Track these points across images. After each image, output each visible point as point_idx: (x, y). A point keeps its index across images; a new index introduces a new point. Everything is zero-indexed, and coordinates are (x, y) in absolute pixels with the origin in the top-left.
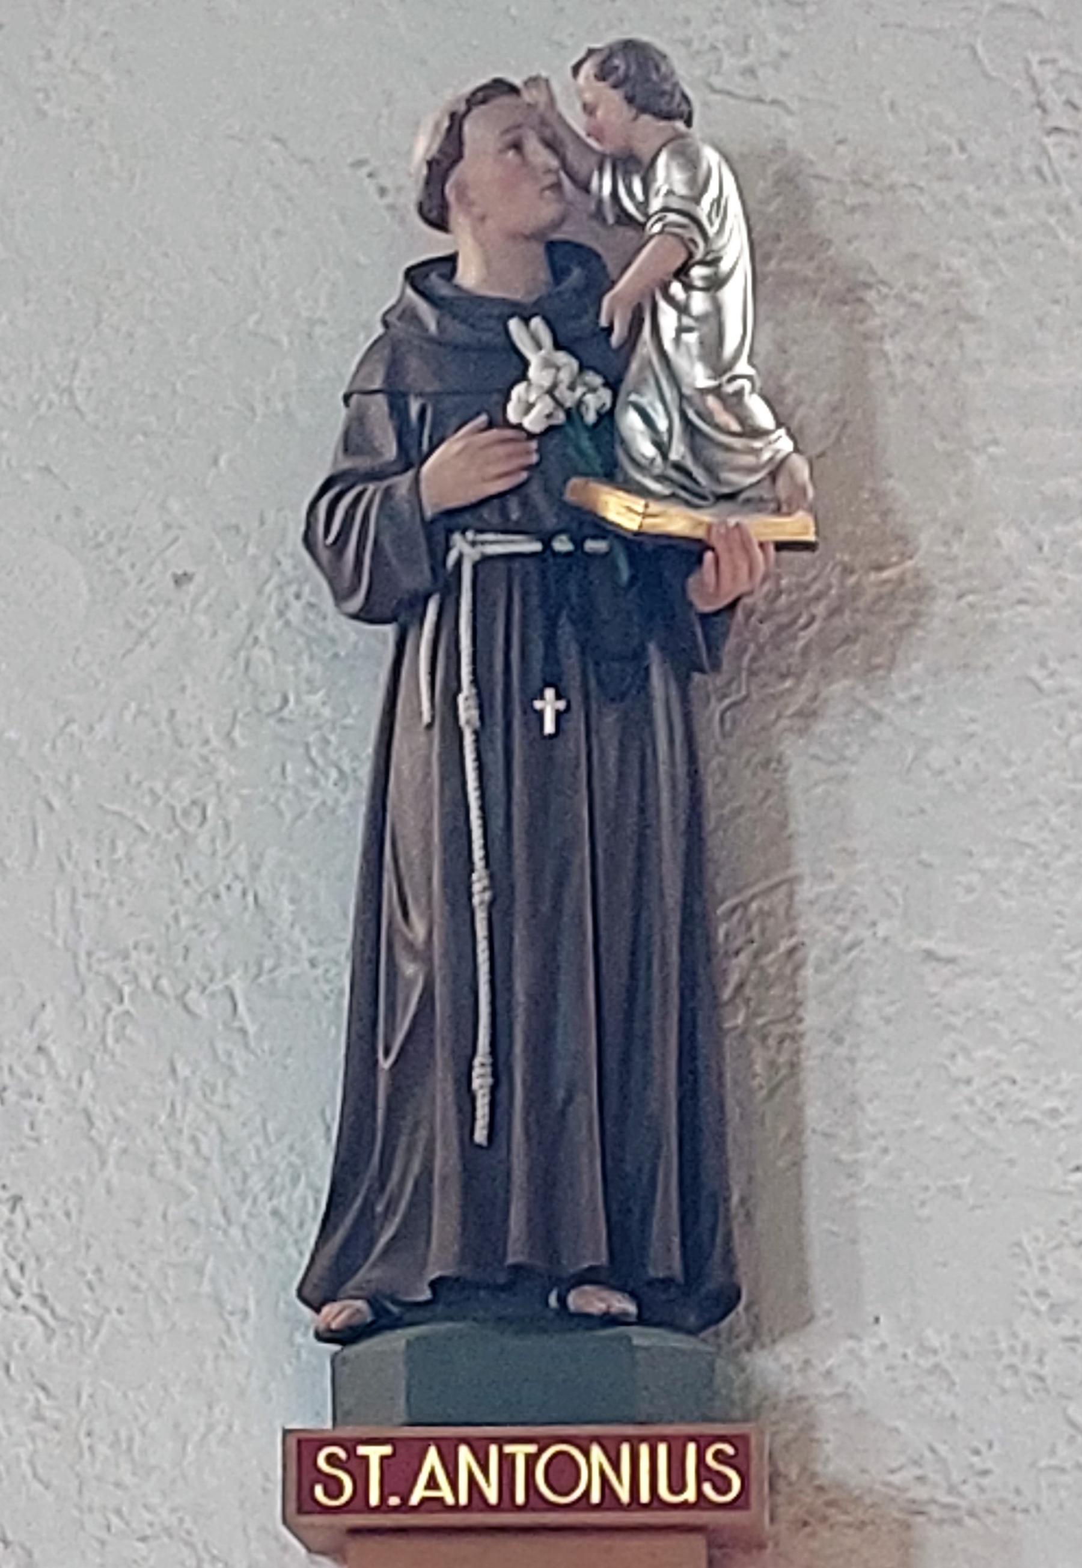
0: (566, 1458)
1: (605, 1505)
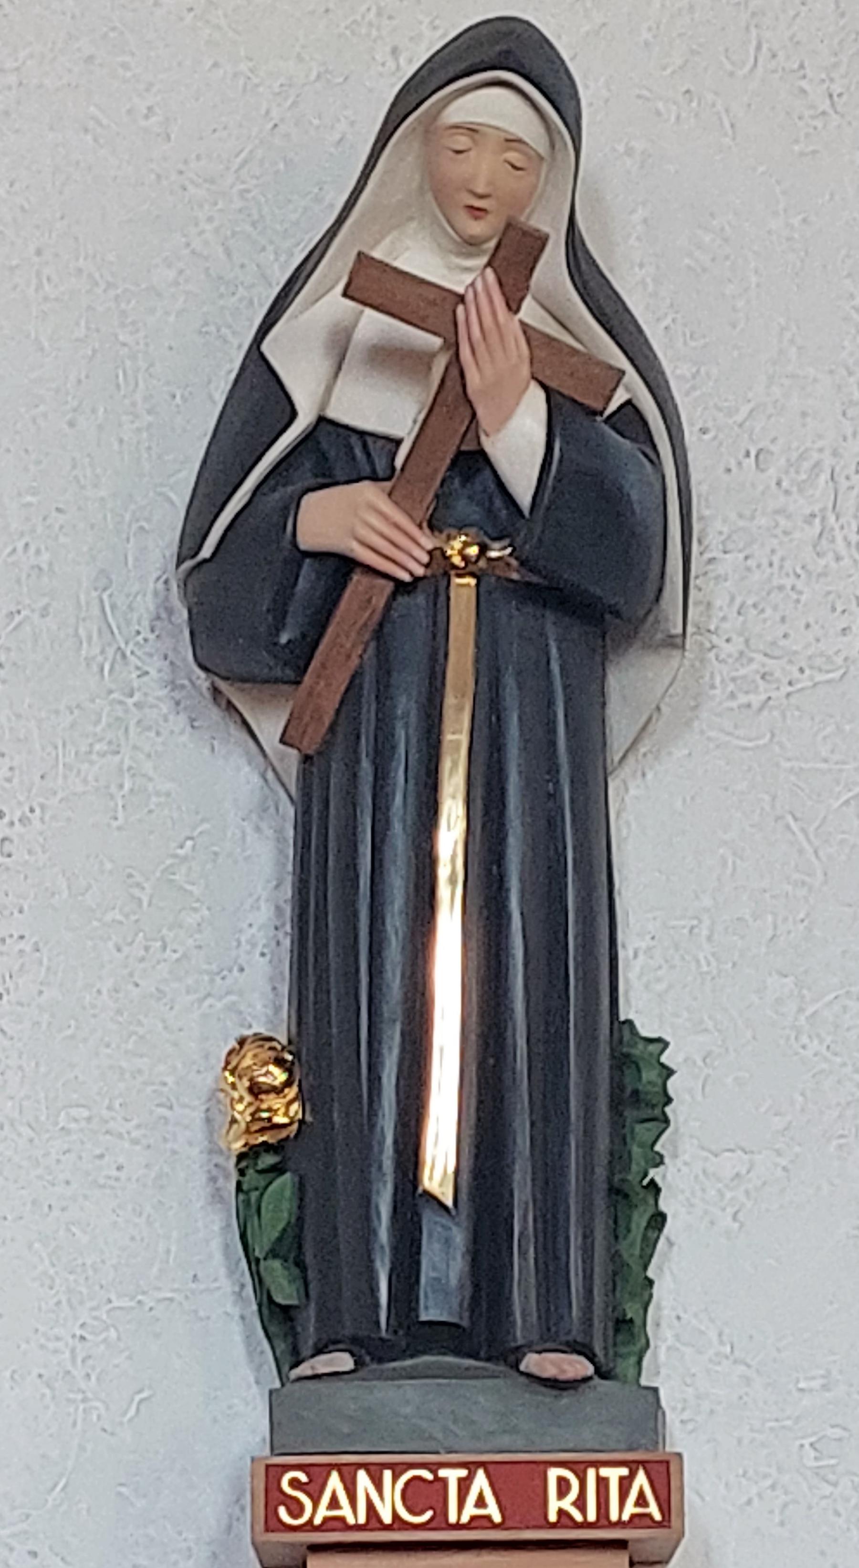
0: (417, 1482)
1: (600, 1524)
